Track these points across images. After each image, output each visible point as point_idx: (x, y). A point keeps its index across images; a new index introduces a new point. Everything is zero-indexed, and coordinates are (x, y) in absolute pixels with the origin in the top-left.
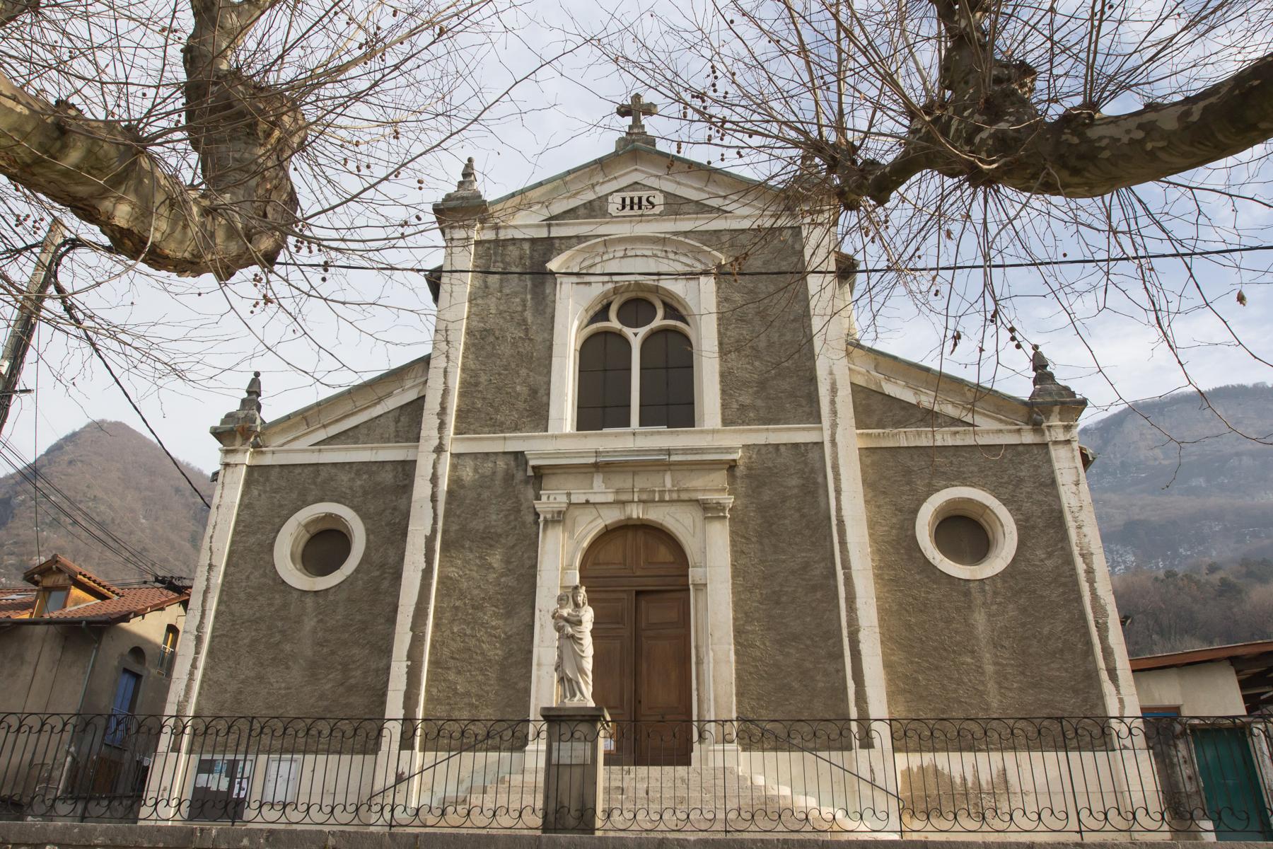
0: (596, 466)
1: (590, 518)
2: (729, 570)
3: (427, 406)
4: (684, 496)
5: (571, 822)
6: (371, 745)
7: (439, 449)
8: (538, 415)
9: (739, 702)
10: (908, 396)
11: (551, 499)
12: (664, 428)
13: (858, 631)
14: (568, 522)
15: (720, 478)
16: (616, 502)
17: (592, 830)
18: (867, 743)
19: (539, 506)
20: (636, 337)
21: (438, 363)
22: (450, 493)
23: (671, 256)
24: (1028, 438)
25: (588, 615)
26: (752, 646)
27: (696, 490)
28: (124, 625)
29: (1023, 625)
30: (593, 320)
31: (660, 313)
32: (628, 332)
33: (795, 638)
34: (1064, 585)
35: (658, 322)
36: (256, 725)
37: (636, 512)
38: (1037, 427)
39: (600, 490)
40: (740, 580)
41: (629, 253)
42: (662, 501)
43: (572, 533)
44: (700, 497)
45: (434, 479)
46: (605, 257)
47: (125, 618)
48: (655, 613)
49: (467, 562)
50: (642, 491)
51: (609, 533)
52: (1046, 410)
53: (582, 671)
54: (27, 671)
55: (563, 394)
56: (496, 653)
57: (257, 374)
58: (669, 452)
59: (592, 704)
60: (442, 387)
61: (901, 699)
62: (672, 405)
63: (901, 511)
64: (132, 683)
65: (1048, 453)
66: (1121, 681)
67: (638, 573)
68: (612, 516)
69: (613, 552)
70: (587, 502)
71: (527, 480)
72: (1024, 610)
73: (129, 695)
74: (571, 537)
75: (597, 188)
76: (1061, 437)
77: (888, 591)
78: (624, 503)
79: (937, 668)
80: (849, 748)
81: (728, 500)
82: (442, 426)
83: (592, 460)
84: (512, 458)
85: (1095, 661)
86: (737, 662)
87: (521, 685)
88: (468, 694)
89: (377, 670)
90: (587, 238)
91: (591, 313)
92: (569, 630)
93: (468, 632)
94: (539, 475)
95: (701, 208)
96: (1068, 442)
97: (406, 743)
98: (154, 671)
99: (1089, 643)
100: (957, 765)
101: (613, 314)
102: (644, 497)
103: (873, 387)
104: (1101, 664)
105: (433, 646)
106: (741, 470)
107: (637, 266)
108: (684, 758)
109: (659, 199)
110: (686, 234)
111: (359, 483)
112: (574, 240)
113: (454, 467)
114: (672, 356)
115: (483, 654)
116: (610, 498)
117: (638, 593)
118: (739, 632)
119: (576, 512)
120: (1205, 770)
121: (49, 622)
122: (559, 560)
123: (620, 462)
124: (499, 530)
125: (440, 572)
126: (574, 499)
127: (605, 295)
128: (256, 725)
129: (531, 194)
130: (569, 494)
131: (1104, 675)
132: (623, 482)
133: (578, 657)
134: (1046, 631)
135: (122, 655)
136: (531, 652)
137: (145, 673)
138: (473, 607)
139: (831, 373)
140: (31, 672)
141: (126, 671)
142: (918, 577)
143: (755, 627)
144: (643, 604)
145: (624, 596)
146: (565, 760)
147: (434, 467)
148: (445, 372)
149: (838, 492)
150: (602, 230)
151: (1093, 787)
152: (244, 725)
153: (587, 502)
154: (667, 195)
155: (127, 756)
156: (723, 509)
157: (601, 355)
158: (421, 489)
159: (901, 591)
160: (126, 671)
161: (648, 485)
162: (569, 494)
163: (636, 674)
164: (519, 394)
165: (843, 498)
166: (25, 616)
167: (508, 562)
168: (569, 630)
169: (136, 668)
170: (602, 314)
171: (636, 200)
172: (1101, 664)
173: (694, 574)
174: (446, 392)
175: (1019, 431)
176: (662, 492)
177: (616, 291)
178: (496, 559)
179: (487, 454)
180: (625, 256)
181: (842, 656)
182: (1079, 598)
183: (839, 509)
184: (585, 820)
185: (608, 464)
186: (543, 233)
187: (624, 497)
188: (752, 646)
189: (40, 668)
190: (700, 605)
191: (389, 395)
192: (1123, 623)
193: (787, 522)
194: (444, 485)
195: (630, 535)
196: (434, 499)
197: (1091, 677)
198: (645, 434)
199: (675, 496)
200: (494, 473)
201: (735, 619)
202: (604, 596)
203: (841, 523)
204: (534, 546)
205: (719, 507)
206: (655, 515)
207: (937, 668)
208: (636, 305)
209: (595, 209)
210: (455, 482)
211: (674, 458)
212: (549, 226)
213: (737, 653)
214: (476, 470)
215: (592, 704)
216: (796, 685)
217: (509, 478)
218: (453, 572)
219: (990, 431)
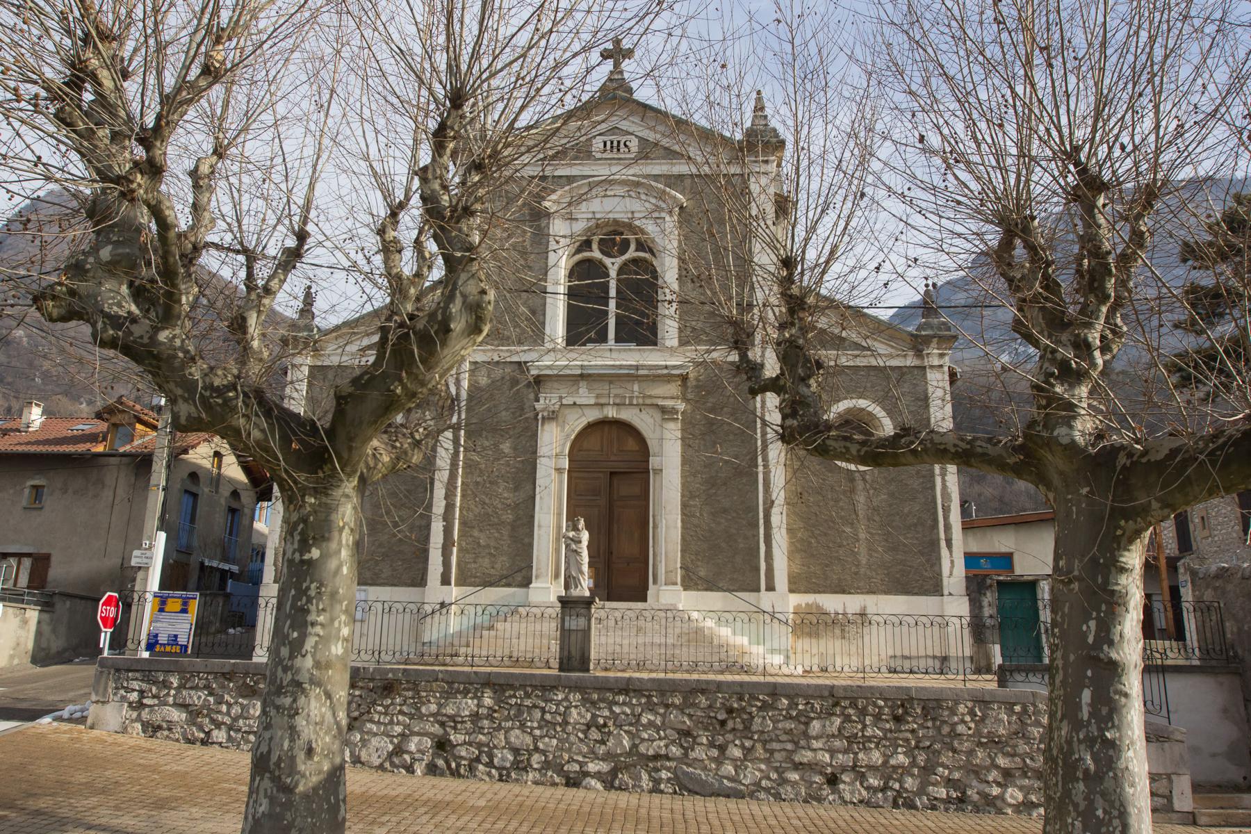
0: (582, 376)
1: (577, 416)
2: (679, 459)
4: (648, 401)
5: (576, 664)
6: (420, 581)
8: (536, 333)
9: (682, 557)
11: (547, 400)
12: (633, 346)
14: (560, 420)
15: (673, 389)
16: (596, 404)
17: (588, 670)
18: (771, 588)
19: (538, 406)
20: (613, 265)
23: (643, 197)
24: (910, 361)
25: (585, 536)
26: (694, 516)
28: (183, 456)
29: (890, 505)
30: (578, 251)
31: (633, 246)
32: (608, 261)
33: (725, 511)
34: (924, 477)
35: (631, 253)
36: (386, 606)
37: (611, 413)
38: (919, 354)
39: (584, 395)
40: (687, 468)
41: (609, 193)
42: (631, 404)
44: (661, 402)
47: (185, 451)
48: (626, 488)
50: (616, 396)
51: (591, 427)
52: (927, 340)
53: (582, 573)
54: (107, 494)
55: (555, 315)
56: (508, 517)
58: (637, 368)
59: (587, 594)
61: (798, 556)
62: (640, 331)
64: (191, 500)
65: (925, 374)
66: (954, 548)
67: (613, 458)
68: (593, 415)
69: (593, 442)
71: (529, 385)
72: (892, 495)
73: (189, 511)
74: (562, 430)
76: (936, 362)
78: (602, 405)
79: (825, 534)
80: (758, 590)
81: (681, 406)
83: (579, 372)
84: (516, 367)
85: (938, 534)
86: (683, 528)
87: (526, 540)
88: (488, 546)
89: (420, 527)
92: (574, 546)
93: (487, 501)
95: (670, 154)
96: (941, 366)
97: (445, 581)
98: (207, 490)
99: (936, 520)
100: (832, 603)
101: (595, 246)
102: (618, 401)
104: (942, 535)
106: (692, 382)
107: (614, 207)
108: (640, 594)
109: (634, 144)
110: (656, 177)
112: (564, 181)
113: (472, 372)
114: (641, 286)
116: (592, 401)
117: (611, 473)
118: (684, 506)
119: (567, 411)
120: (1000, 609)
121: (123, 455)
122: (553, 443)
123: (599, 375)
126: (564, 402)
127: (589, 229)
128: (386, 606)
131: (943, 544)
132: (603, 388)
133: (579, 565)
134: (906, 510)
135: (183, 480)
136: (533, 517)
137: (200, 493)
138: (490, 483)
140: (111, 493)
141: (186, 491)
143: (697, 502)
144: (615, 482)
145: (601, 475)
146: (573, 627)
150: (586, 171)
151: (875, 651)
152: (379, 606)
154: (640, 139)
155: (192, 558)
156: (677, 413)
157: (585, 272)
160: (186, 491)
161: (620, 391)
163: (610, 532)
166: (100, 448)
167: (515, 449)
168: (574, 546)
169: (194, 489)
170: (586, 245)
171: (615, 144)
172: (942, 535)
173: (654, 462)
175: (905, 356)
176: (631, 398)
178: (506, 447)
181: (757, 526)
182: (933, 487)
184: (584, 664)
185: (590, 375)
187: (602, 401)
188: (694, 516)
189: (120, 491)
190: (657, 484)
192: (962, 506)
195: (606, 429)
197: (935, 544)
198: (619, 351)
199: (641, 401)
201: (683, 496)
202: (585, 475)
204: (534, 436)
205: (674, 411)
206: (626, 415)
207: (825, 534)
208: (614, 236)
209: (583, 152)
210: (474, 387)
211: (641, 372)
213: (682, 521)
214: (489, 376)
215: (587, 594)
216: (723, 545)
219: (886, 355)
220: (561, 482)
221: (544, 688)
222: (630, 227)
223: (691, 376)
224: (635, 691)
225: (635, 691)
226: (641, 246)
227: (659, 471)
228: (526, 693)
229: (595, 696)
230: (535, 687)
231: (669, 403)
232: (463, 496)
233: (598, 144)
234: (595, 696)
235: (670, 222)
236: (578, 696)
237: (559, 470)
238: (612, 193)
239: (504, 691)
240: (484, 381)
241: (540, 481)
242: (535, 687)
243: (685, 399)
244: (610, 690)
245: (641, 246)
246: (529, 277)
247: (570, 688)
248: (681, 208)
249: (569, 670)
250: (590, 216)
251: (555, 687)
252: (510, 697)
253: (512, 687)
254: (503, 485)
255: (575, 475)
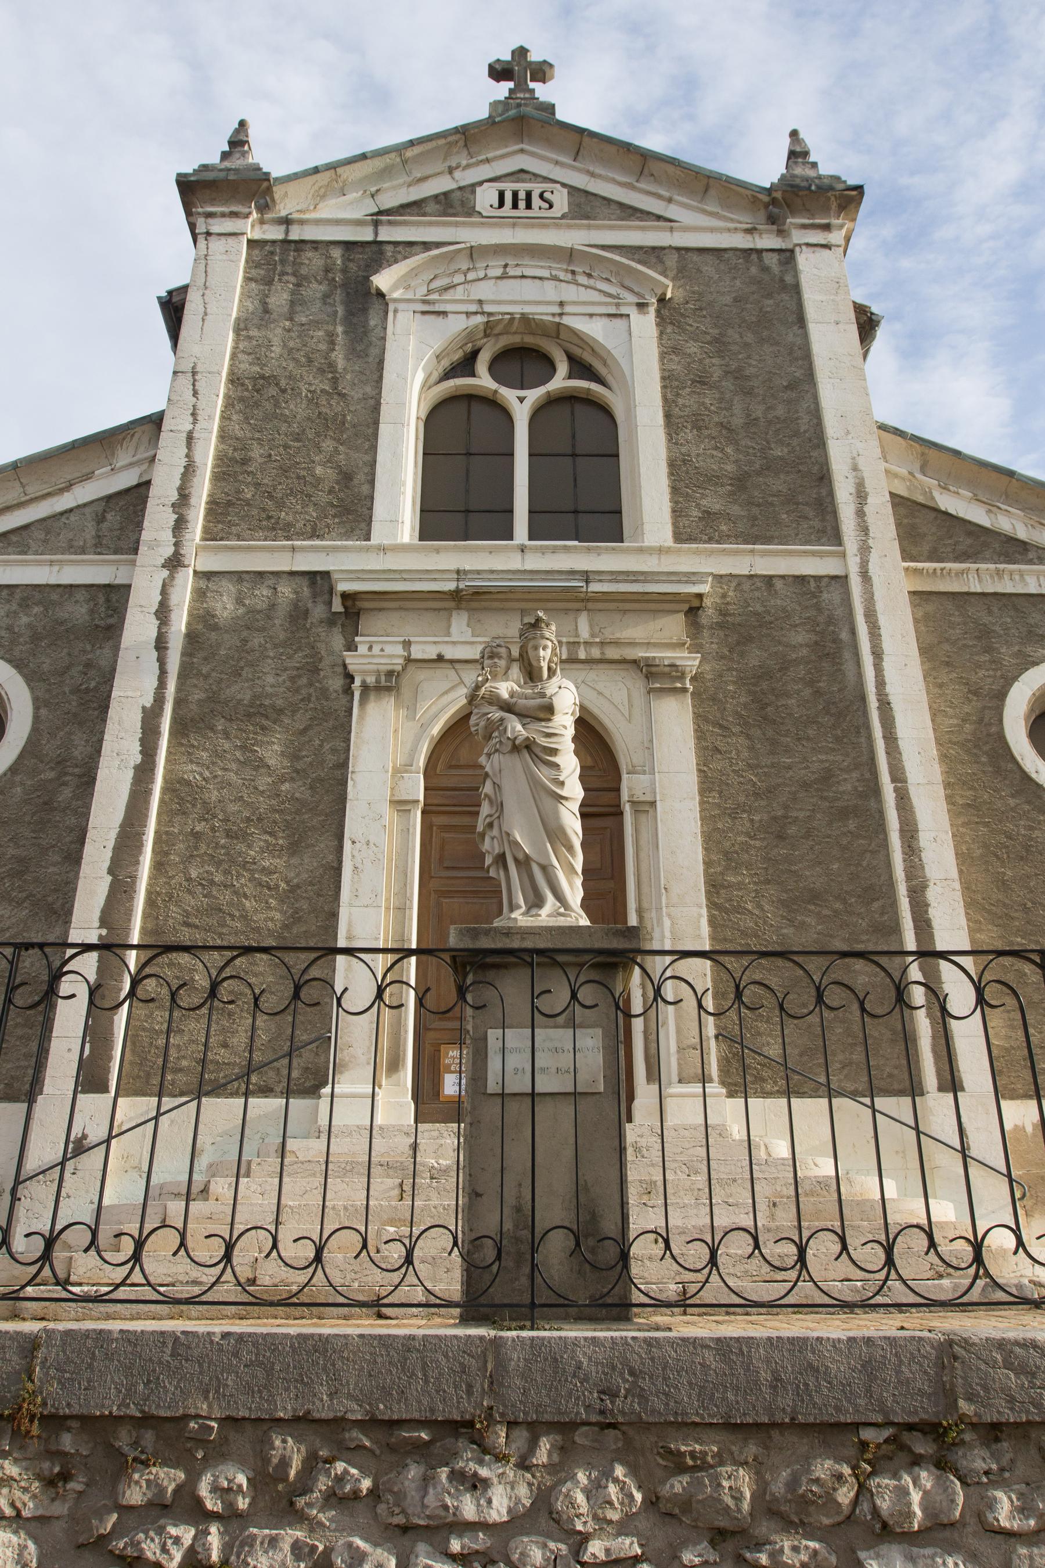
0: (456, 596)
1: (446, 685)
3: (153, 491)
4: (612, 653)
7: (175, 563)
8: (353, 513)
10: (977, 515)
11: (374, 651)
13: (924, 887)
14: (406, 691)
15: (674, 626)
19: (352, 661)
20: (521, 404)
21: (177, 424)
22: (191, 637)
23: (582, 279)
26: (739, 910)
27: (632, 644)
32: (509, 395)
33: (814, 897)
39: (463, 637)
40: (714, 798)
41: (511, 272)
43: (412, 709)
45: (163, 613)
46: (471, 276)
49: (218, 754)
53: (556, 835)
55: (395, 505)
57: (794, 134)
58: (587, 576)
60: (183, 462)
63: (976, 693)
70: (440, 658)
75: (457, 174)
77: (964, 824)
81: (690, 661)
82: (180, 525)
83: (451, 586)
84: (305, 582)
90: (427, 246)
91: (446, 363)
93: (218, 878)
94: (354, 611)
97: (90, 1078)
101: (482, 365)
103: (921, 499)
105: (150, 902)
106: (709, 615)
109: (561, 201)
111: (24, 620)
115: (244, 917)
118: (714, 886)
119: (422, 675)
124: (280, 703)
125: (168, 771)
126: (417, 653)
127: (470, 335)
129: (345, 172)
130: (407, 644)
136: (334, 915)
138: (228, 834)
139: (855, 468)
142: (1012, 802)
147: (164, 592)
148: (190, 438)
149: (878, 655)
153: (440, 658)
156: (682, 677)
158: (139, 628)
159: (986, 825)
162: (407, 644)
164: (319, 480)
165: (887, 664)
170: (466, 365)
174: (189, 470)
177: (488, 330)
179: (261, 574)
180: (504, 277)
183: (881, 683)
184: (604, 1286)
186: (366, 235)
188: (739, 910)
190: (645, 836)
191: (88, 477)
193: (792, 702)
194: (180, 623)
196: (161, 645)
199: (596, 653)
200: (272, 606)
201: (708, 864)
203: (885, 705)
204: (343, 730)
205: (675, 672)
208: (523, 353)
209: (454, 204)
211: (595, 587)
212: (376, 224)
213: (712, 922)
214: (239, 601)
217: (298, 615)
218: (191, 772)
220: (406, 832)
221: (390, 1438)
222: (557, 331)
223: (707, 602)
224: (993, 1432)
225: (993, 1432)
226: (580, 368)
227: (646, 807)
228: (267, 1479)
229: (738, 1485)
230: (328, 1432)
231: (667, 655)
232: (159, 866)
233: (486, 198)
234: (738, 1485)
235: (645, 326)
236: (624, 1490)
237: (401, 805)
238: (518, 272)
239: (120, 1468)
240: (225, 605)
241: (354, 825)
242: (328, 1432)
243: (696, 648)
244: (831, 1432)
245: (580, 368)
246: (307, 1550)
247: (565, 1428)
248: (662, 300)
249: (529, 1313)
250: (473, 308)
251: (464, 1429)
252: (160, 1509)
253: (174, 1437)
254: (260, 839)
255: (439, 820)
